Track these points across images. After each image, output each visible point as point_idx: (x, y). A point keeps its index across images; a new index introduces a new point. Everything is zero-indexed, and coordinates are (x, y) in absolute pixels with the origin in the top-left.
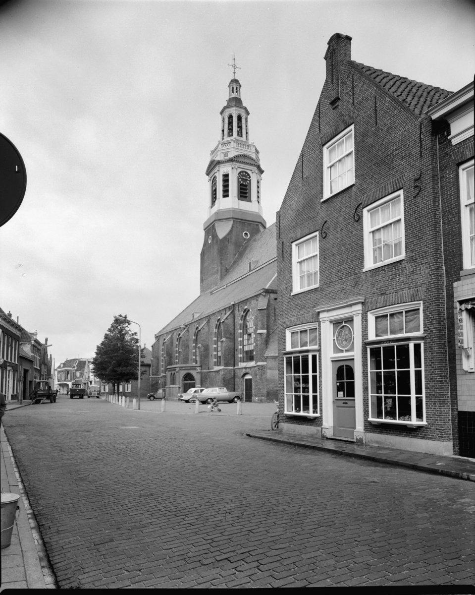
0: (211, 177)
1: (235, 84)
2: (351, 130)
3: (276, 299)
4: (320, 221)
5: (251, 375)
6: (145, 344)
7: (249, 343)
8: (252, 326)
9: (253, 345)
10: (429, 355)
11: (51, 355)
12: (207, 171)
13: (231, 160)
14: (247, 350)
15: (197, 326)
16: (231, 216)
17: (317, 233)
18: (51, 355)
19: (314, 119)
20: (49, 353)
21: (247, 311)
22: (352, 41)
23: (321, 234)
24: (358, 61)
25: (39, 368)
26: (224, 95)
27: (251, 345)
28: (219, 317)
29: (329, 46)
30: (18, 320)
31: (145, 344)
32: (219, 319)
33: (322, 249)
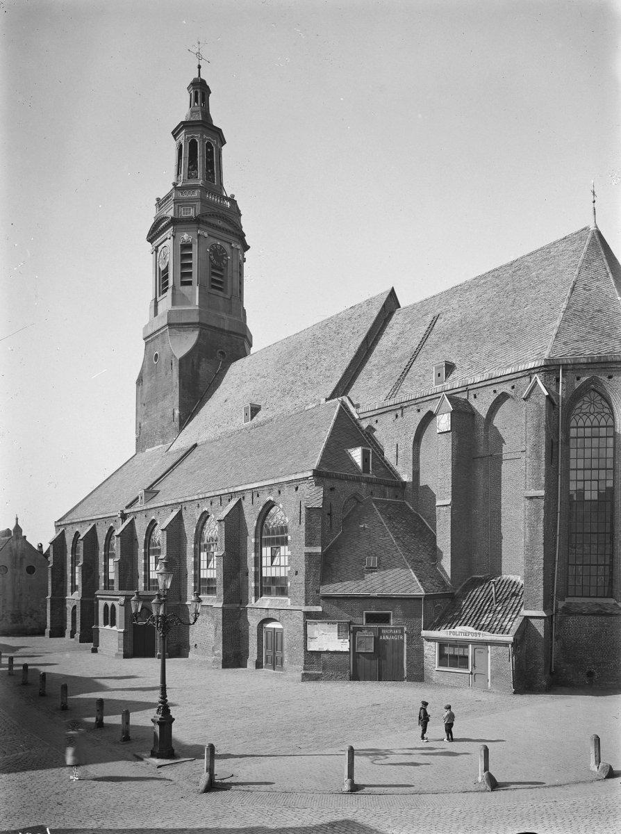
0: (157, 247)
1: (200, 90)
12: (149, 235)
13: (197, 221)
16: (197, 320)
26: (182, 110)
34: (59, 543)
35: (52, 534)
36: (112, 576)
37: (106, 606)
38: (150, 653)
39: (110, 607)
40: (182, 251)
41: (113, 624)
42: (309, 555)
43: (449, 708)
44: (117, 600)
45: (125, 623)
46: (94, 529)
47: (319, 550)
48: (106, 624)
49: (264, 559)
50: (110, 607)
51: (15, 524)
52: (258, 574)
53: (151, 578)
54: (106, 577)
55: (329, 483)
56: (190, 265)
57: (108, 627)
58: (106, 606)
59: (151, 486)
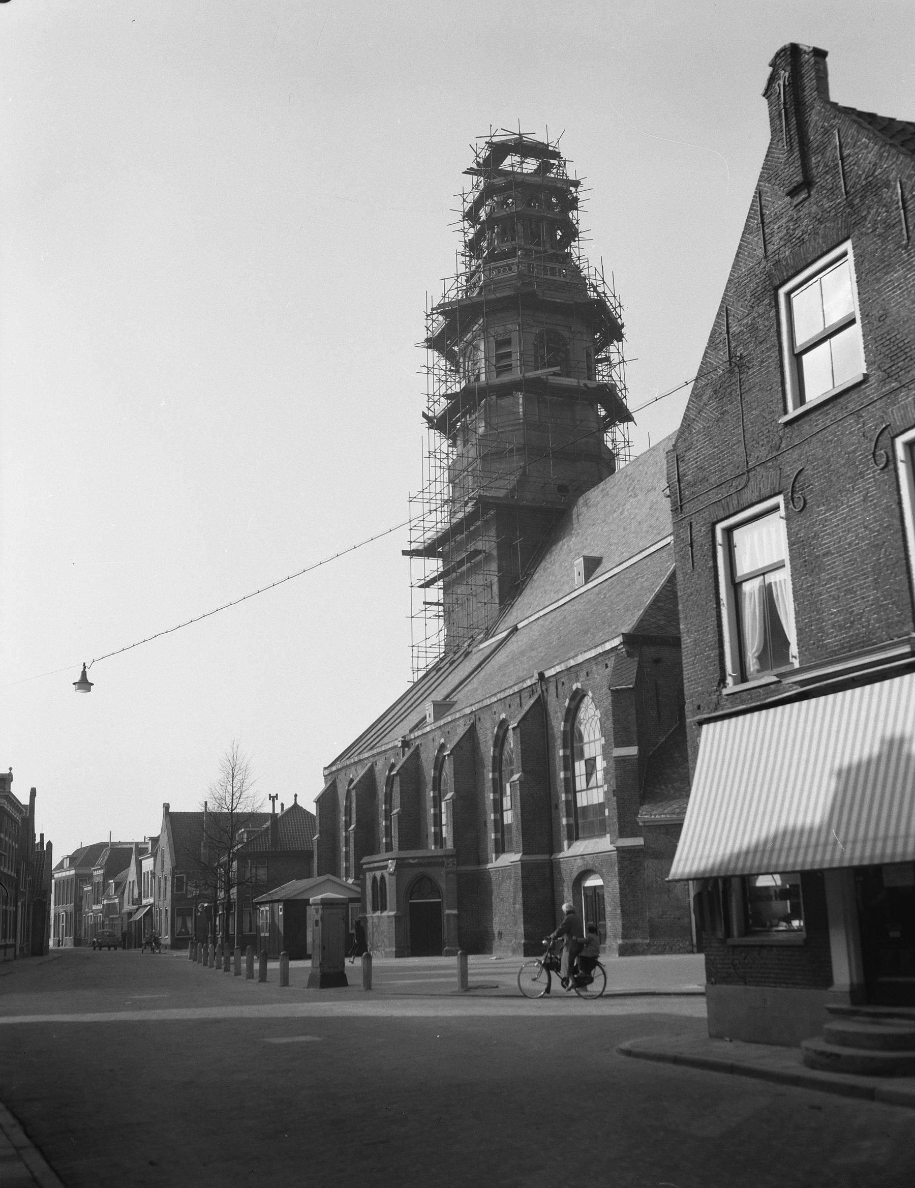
2: (845, 254)
3: (657, 661)
4: (790, 471)
5: (602, 877)
6: (296, 796)
7: (592, 784)
8: (598, 735)
9: (601, 790)
10: (748, 496)
11: (42, 835)
14: (585, 804)
15: (442, 740)
17: (780, 499)
18: (42, 835)
19: (747, 229)
20: (38, 832)
21: (578, 697)
22: (828, 59)
23: (788, 502)
24: (843, 103)
25: (13, 874)
27: (595, 791)
28: (503, 716)
29: (774, 71)
30: (558, 975)
31: (296, 796)
32: (504, 721)
33: (796, 543)
34: (327, 800)
35: (319, 786)
36: (508, 818)
37: (375, 879)
38: (435, 950)
39: (378, 879)
40: (497, 349)
41: (384, 908)
42: (621, 761)
43: (11, 769)
44: (386, 867)
45: (398, 902)
46: (371, 770)
47: (633, 751)
48: (375, 909)
49: (577, 779)
50: (378, 879)
51: (293, 803)
52: (571, 804)
53: (579, 805)
54: (499, 822)
55: (650, 652)
56: (509, 355)
57: (378, 913)
58: (375, 879)
59: (448, 696)
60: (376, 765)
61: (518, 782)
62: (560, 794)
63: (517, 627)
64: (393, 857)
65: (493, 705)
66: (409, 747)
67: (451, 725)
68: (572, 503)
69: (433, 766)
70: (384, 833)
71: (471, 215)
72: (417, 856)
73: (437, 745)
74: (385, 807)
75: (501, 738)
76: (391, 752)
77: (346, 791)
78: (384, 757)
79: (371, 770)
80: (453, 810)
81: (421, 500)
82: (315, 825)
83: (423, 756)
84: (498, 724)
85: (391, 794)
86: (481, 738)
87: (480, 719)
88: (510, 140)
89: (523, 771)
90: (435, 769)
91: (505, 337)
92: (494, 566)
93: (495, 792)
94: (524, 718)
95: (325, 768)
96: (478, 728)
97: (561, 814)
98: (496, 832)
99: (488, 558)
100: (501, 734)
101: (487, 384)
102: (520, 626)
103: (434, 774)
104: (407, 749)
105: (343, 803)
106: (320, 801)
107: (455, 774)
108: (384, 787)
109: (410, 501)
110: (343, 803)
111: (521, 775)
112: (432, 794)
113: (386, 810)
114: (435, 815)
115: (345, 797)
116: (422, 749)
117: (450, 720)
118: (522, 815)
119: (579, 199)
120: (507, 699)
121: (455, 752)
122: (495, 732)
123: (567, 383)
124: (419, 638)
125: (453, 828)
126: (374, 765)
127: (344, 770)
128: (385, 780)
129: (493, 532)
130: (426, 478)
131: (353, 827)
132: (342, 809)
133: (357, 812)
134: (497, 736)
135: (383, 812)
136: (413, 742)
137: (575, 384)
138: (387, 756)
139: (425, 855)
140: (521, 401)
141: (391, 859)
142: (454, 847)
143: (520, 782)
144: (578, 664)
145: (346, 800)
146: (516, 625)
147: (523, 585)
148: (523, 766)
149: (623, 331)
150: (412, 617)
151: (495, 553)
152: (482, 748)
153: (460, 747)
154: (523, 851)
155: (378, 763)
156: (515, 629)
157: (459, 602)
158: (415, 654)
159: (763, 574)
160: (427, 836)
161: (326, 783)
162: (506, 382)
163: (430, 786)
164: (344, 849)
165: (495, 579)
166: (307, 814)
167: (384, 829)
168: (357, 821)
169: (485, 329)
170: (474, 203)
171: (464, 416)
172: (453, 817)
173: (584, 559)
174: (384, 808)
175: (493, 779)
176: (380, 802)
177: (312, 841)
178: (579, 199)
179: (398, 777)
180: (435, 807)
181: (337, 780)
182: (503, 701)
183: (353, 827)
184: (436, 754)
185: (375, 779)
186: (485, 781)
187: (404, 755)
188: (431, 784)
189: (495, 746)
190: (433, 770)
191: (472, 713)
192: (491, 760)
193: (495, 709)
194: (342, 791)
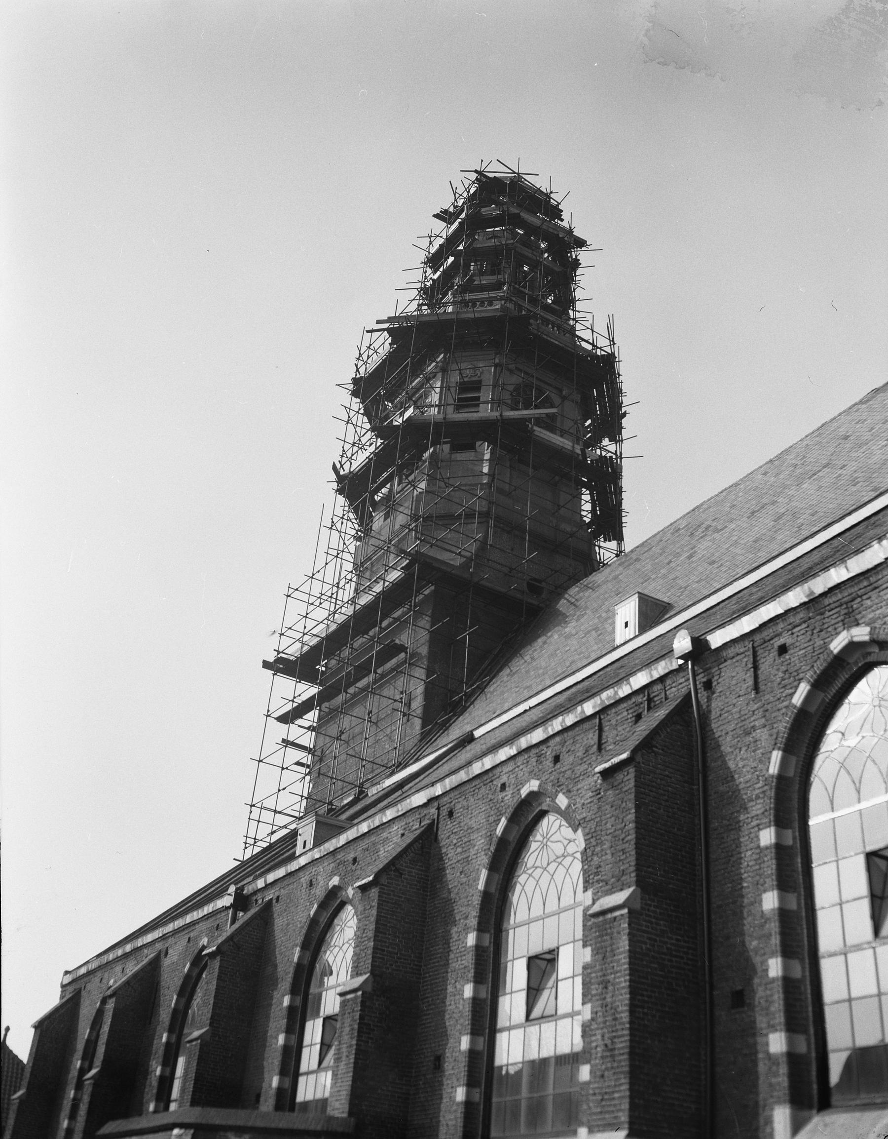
15: (335, 881)
46: (155, 965)
60: (167, 953)
61: (625, 911)
62: (757, 960)
63: (472, 735)
64: (187, 1120)
65: (499, 770)
66: (245, 909)
67: (363, 844)
68: (560, 591)
69: (300, 940)
70: (155, 1091)
71: (434, 261)
72: (250, 1124)
73: (319, 892)
74: (168, 1038)
75: (511, 848)
76: (203, 926)
77: (95, 1011)
78: (187, 937)
79: (155, 965)
80: (361, 1018)
81: (305, 597)
82: (22, 1075)
83: (279, 923)
84: (510, 811)
85: (186, 1013)
86: (451, 854)
87: (451, 814)
88: (506, 178)
89: (639, 883)
90: (304, 946)
91: (474, 379)
92: (420, 673)
93: (478, 980)
94: (645, 746)
95: (67, 973)
96: (442, 834)
97: (761, 1022)
98: (470, 1084)
99: (413, 659)
100: (513, 837)
101: (444, 418)
102: (477, 734)
103: (300, 958)
104: (241, 914)
105: (84, 1032)
106: (44, 1028)
107: (377, 930)
108: (175, 997)
109: (288, 596)
110: (84, 1032)
111: (634, 891)
112: (286, 1001)
113: (168, 1043)
114: (286, 1048)
115: (90, 1022)
116: (277, 908)
117: (366, 830)
118: (632, 1012)
119: (580, 264)
120: (552, 743)
121: (383, 880)
122: (499, 830)
123: (558, 443)
124: (263, 792)
125: (355, 1063)
126: (162, 955)
127: (99, 974)
128: (180, 983)
129: (425, 622)
130: (323, 548)
131: (93, 1072)
132: (80, 1046)
133: (108, 1044)
134: (502, 841)
135: (162, 1048)
136: (259, 896)
137: (569, 448)
138: (192, 935)
139: (273, 1125)
140: (487, 456)
141: (181, 1126)
142: (351, 1113)
143: (630, 912)
144: (868, 571)
145: (92, 1028)
146: (472, 732)
147: (466, 701)
148: (639, 867)
149: (624, 421)
150: (260, 761)
151: (424, 650)
152: (449, 877)
153: (397, 870)
154: (631, 1123)
155: (170, 951)
156: (469, 739)
157: (343, 737)
158: (255, 815)
159: (529, 924)
160: (258, 1096)
161: (62, 997)
162: (473, 419)
163: (285, 984)
164: (65, 1124)
165: (420, 689)
166: (18, 1064)
167: (155, 1083)
168: (105, 1062)
169: (444, 370)
170: (447, 239)
171: (390, 479)
172: (359, 1036)
173: (640, 598)
174: (164, 1039)
175: (478, 947)
176: (159, 1028)
177: (9, 1099)
178: (580, 264)
179: (218, 958)
180: (289, 1031)
181: (83, 993)
182: (534, 751)
183: (93, 1072)
184: (312, 913)
185: (158, 983)
186: (452, 956)
187: (233, 922)
188: (289, 978)
189: (493, 867)
190: (298, 949)
191: (430, 801)
192: (476, 900)
193: (504, 779)
194: (87, 1012)
